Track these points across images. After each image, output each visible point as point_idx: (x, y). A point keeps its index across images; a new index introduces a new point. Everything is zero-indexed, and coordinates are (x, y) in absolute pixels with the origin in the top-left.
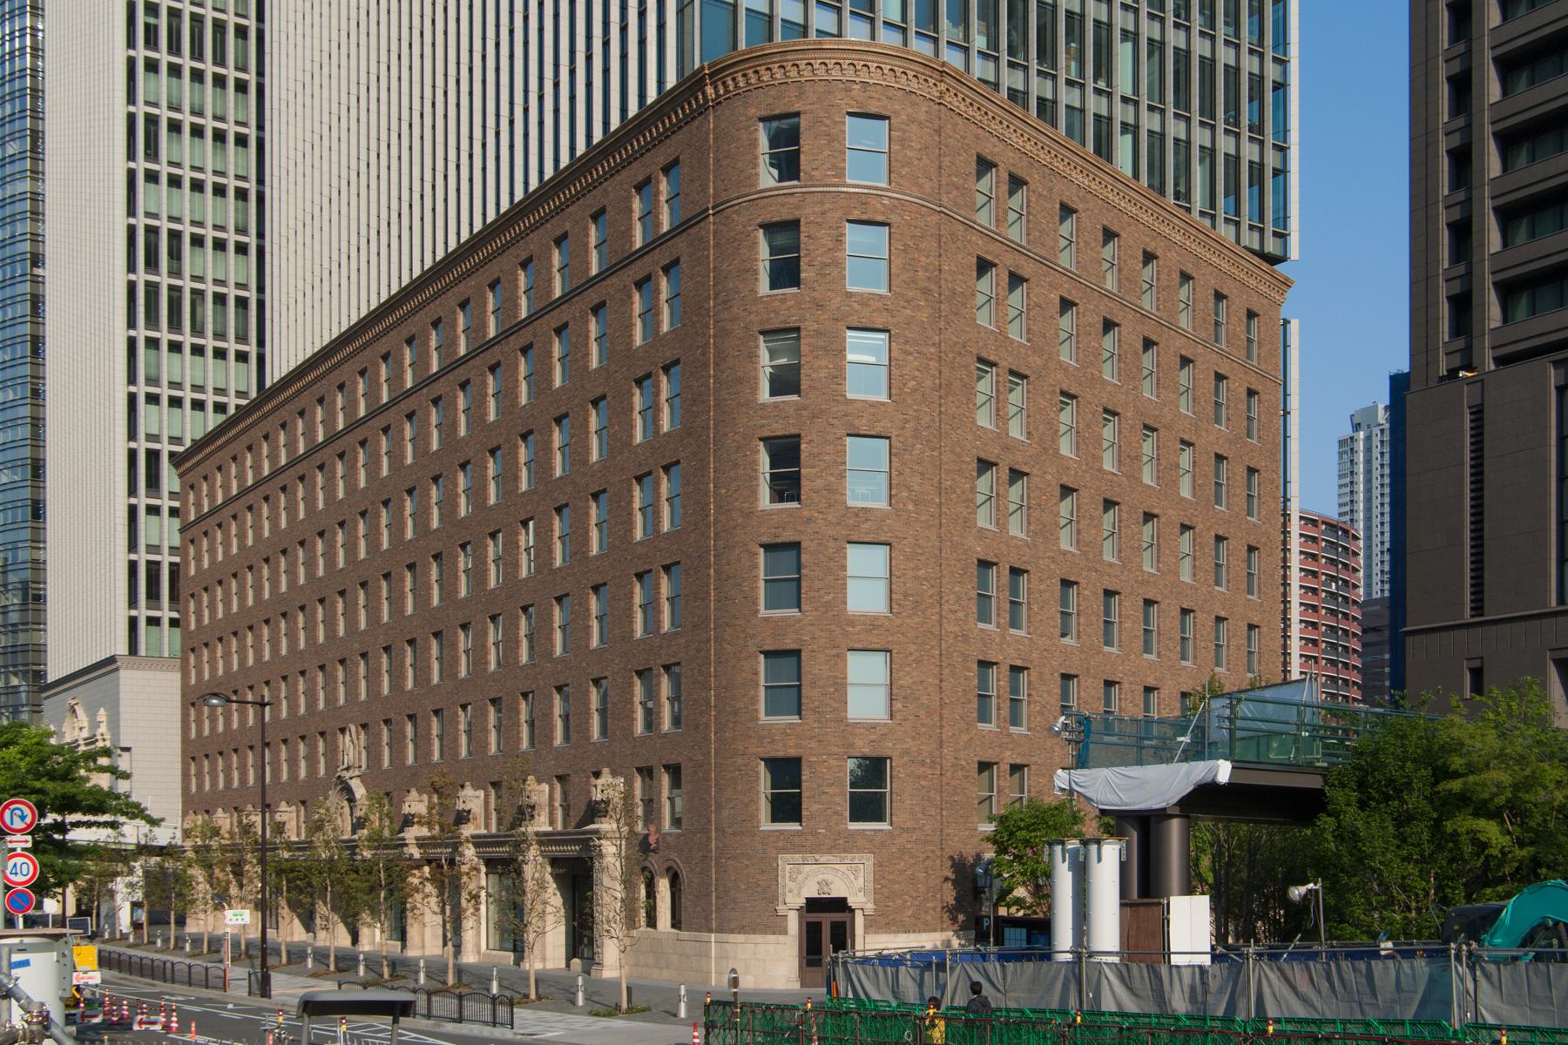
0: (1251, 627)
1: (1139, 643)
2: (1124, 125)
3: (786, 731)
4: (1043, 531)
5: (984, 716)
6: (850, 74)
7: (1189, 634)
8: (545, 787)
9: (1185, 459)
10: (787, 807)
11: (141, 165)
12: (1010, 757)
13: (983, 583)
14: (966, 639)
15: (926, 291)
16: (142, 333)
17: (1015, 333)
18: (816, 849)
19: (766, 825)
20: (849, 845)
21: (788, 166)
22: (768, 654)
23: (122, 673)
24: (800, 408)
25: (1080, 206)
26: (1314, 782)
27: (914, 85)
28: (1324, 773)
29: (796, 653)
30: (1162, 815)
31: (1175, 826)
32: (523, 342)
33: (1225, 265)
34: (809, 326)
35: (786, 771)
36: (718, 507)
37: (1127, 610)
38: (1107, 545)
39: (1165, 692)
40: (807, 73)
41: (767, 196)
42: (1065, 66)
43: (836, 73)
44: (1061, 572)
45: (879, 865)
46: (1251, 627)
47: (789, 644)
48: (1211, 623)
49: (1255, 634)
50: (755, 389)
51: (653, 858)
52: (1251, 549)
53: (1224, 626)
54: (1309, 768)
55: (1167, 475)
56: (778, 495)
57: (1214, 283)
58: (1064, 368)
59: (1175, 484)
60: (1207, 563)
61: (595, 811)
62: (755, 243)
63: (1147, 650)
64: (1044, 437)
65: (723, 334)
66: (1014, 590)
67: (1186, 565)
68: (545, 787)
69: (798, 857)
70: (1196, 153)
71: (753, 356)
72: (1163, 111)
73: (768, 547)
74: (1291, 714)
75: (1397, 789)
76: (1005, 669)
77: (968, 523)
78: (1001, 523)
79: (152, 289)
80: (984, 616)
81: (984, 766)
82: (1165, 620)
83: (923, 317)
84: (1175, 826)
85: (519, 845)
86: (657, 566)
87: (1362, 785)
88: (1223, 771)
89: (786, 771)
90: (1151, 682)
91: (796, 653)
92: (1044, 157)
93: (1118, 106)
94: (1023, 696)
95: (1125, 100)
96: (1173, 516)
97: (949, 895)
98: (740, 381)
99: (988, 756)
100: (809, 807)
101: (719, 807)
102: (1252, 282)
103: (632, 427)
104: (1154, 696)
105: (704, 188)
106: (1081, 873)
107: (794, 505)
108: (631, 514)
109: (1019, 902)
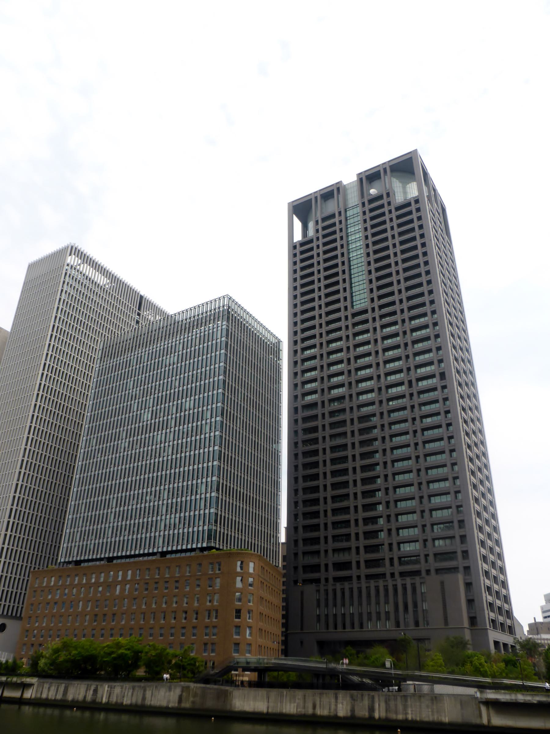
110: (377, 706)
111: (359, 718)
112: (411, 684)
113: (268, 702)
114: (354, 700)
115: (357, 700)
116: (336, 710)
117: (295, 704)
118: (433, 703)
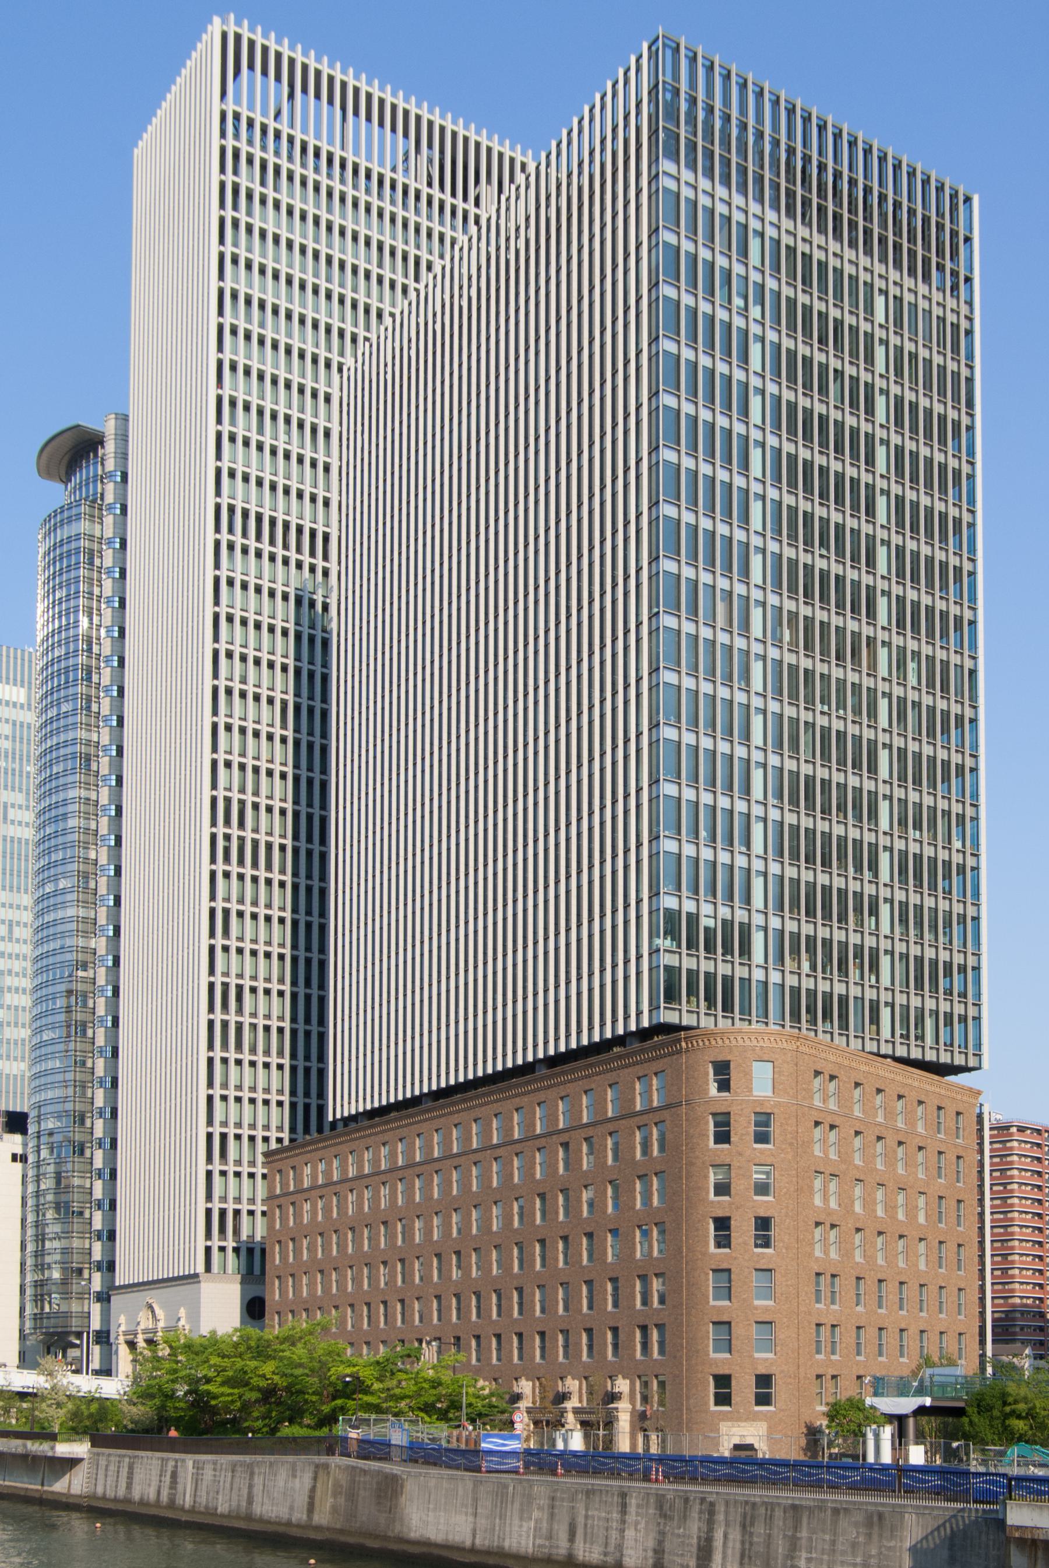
0: (960, 1290)
1: (897, 1306)
2: (883, 591)
3: (724, 1361)
4: (847, 1253)
5: (818, 1352)
6: (755, 1043)
7: (924, 1298)
8: (577, 1382)
9: (921, 1201)
10: (723, 1399)
11: (219, 941)
12: (831, 1372)
13: (818, 1284)
14: (810, 1314)
15: (791, 1144)
16: (218, 1054)
17: (833, 1156)
18: (739, 1419)
19: (713, 1408)
20: (754, 1417)
21: (724, 1085)
22: (714, 1323)
23: (203, 1285)
24: (730, 1204)
25: (864, 1081)
26: (961, 1404)
27: (785, 1045)
28: (966, 1401)
29: (729, 1323)
30: (906, 1416)
31: (911, 1421)
32: (562, 1140)
33: (943, 1092)
34: (735, 1164)
35: (723, 1381)
36: (688, 1249)
37: (891, 1289)
38: (879, 1254)
39: (911, 1331)
40: (734, 1042)
41: (714, 1100)
42: (854, 974)
43: (748, 1043)
44: (855, 1274)
45: (769, 1428)
46: (960, 1290)
47: (725, 1319)
48: (937, 1290)
49: (962, 1293)
50: (708, 1193)
51: (648, 1423)
52: (959, 1245)
53: (944, 1291)
54: (960, 1399)
55: (911, 1211)
56: (719, 1245)
57: (937, 1102)
58: (857, 1167)
59: (916, 1217)
60: (934, 1257)
61: (614, 1397)
62: (707, 1123)
63: (901, 1308)
64: (846, 1203)
65: (690, 1164)
66: (833, 1284)
67: (922, 1259)
68: (577, 1382)
69: (730, 1424)
70: (927, 1013)
71: (707, 1177)
72: (920, 741)
73: (714, 1271)
74: (953, 1380)
75: (990, 1408)
76: (829, 1327)
77: (811, 1255)
78: (826, 1252)
79: (225, 1024)
80: (818, 1301)
81: (819, 1377)
82: (911, 1291)
83: (790, 1157)
84: (911, 1421)
85: (563, 1412)
86: (651, 1273)
87: (978, 1406)
88: (928, 1401)
89: (723, 1381)
90: (903, 1326)
91: (729, 1323)
92: (846, 1063)
93: (879, 580)
94: (837, 1339)
95: (883, 628)
96: (916, 1234)
97: (803, 1442)
98: (699, 1188)
99: (820, 1372)
100: (735, 1399)
101: (688, 1398)
102: (959, 1097)
103: (635, 1199)
104: (905, 1334)
105: (680, 1090)
106: (877, 1436)
107: (727, 1250)
108: (634, 1244)
109: (838, 1445)
110: (719, 1535)
111: (261, 1520)
112: (209, 1461)
113: (475, 1515)
114: (664, 1516)
115: (671, 1518)
116: (620, 1547)
117: (532, 1524)
118: (869, 1536)
